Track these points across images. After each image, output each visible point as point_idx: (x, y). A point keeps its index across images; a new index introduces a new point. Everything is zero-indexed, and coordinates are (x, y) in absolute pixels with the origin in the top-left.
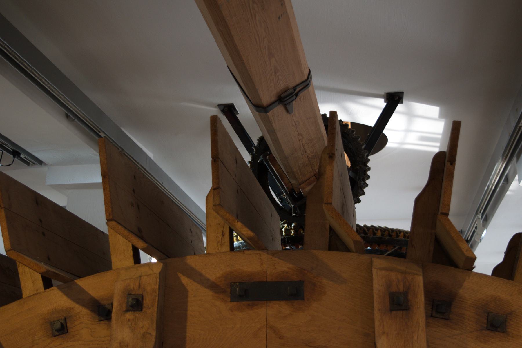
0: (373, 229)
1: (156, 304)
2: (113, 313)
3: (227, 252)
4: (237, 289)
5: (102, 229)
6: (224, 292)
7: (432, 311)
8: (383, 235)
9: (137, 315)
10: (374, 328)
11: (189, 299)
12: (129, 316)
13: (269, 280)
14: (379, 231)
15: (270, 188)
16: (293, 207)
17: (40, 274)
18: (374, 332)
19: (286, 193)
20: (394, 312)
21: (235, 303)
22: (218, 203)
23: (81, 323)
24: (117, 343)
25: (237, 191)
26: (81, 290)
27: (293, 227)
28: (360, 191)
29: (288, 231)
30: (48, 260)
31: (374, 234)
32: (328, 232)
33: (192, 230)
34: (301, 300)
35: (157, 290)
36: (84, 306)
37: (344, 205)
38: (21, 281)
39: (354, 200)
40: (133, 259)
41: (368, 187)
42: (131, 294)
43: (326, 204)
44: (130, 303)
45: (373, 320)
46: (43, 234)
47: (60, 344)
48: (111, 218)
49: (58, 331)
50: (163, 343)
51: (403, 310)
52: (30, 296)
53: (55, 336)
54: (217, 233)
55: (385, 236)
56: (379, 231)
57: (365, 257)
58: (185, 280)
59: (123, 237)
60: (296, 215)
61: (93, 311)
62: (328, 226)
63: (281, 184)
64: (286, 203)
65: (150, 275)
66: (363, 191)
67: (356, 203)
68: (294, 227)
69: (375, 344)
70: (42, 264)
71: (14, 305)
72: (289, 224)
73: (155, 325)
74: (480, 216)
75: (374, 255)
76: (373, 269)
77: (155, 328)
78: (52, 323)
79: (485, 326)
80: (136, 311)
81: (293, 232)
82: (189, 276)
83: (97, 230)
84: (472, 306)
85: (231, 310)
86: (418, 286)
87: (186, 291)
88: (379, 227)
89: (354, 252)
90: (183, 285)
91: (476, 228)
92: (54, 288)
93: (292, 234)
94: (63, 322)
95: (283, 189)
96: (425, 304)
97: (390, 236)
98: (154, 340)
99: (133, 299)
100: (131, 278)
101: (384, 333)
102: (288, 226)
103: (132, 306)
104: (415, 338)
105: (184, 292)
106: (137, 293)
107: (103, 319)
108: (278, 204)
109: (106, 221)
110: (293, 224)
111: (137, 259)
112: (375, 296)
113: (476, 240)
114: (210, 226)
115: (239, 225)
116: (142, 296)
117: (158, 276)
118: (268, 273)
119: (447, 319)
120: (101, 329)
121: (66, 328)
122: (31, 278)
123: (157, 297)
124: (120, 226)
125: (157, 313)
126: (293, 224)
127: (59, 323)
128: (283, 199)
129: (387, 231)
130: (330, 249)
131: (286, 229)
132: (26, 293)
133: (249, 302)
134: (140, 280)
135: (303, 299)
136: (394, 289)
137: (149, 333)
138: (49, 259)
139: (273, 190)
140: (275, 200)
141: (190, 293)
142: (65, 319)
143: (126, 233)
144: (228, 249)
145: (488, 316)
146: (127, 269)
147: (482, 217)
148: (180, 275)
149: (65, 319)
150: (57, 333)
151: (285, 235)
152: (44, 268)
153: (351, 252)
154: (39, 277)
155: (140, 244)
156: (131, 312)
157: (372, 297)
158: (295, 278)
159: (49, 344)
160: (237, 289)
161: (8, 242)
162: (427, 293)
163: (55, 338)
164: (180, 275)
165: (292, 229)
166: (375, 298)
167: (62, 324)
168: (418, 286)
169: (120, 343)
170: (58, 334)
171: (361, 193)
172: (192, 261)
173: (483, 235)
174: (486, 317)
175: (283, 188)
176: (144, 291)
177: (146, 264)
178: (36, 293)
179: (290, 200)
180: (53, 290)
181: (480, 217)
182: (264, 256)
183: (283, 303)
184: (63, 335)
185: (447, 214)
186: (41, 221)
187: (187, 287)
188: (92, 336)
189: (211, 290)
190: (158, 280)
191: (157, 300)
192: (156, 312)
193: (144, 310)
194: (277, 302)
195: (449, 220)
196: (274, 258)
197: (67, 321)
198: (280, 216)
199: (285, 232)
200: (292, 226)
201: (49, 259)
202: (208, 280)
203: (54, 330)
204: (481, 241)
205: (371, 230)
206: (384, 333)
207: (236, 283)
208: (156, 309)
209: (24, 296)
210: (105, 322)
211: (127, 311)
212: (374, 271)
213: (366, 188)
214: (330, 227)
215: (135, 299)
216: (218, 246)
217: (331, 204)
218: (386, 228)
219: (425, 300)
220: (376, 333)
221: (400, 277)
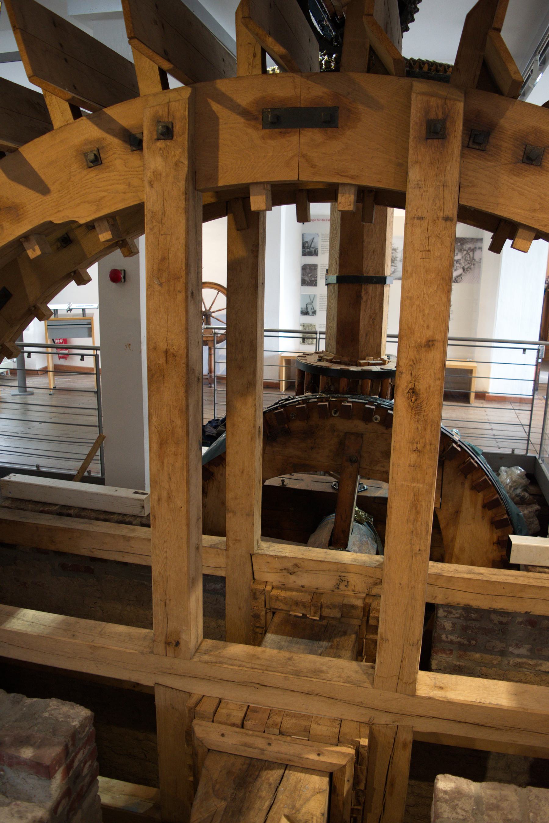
0: (419, 63)
1: (187, 131)
2: (144, 141)
3: (258, 75)
4: (270, 115)
5: (129, 60)
6: (256, 119)
7: (469, 142)
8: (429, 69)
9: (168, 143)
10: (407, 158)
11: (220, 127)
12: (160, 144)
13: (302, 106)
14: (426, 65)
15: (311, 14)
16: (335, 35)
17: (67, 101)
18: (407, 162)
19: (328, 18)
20: (429, 141)
21: (267, 131)
22: (247, 15)
23: (114, 153)
24: (150, 172)
25: (270, 5)
26: (111, 120)
27: (334, 58)
28: (409, 16)
29: (328, 63)
30: (74, 88)
31: (421, 68)
32: (368, 53)
33: (225, 59)
34: (335, 127)
35: (187, 116)
36: (115, 136)
37: (387, 23)
38: (50, 112)
39: (402, 28)
40: (161, 85)
41: (419, 12)
42: (160, 122)
43: (366, 15)
44: (160, 131)
45: (407, 149)
46: (66, 60)
47: (96, 176)
48: (132, 35)
49: (92, 162)
50: (195, 172)
51: (439, 138)
52: (60, 127)
53: (90, 167)
54: (248, 54)
55: (432, 71)
56: (426, 65)
57: (405, 81)
58: (215, 106)
59: (147, 57)
60: (337, 45)
61: (125, 141)
62: (368, 46)
63: (322, 7)
64: (327, 31)
65: (179, 100)
66: (413, 17)
67: (404, 31)
68: (335, 58)
69: (407, 174)
70: (66, 92)
71: (46, 137)
72: (330, 56)
73: (186, 154)
74: (538, 57)
75: (416, 79)
76: (412, 94)
77: (186, 157)
78: (86, 155)
79: (521, 158)
80: (167, 139)
81: (333, 65)
82: (219, 102)
83: (124, 59)
84: (511, 138)
85: (263, 138)
86: (458, 113)
87: (217, 118)
88: (427, 61)
89: (393, 75)
90: (213, 111)
91: (532, 72)
92: (84, 118)
93: (332, 67)
94: (96, 153)
95: (324, 13)
96: (463, 133)
97: (437, 70)
98: (186, 169)
99: (163, 127)
100: (159, 105)
101: (417, 162)
102: (328, 58)
103: (162, 134)
104: (448, 168)
105: (214, 119)
106: (167, 120)
107: (135, 149)
108: (319, 32)
109: (128, 39)
110: (334, 56)
111: (165, 85)
112: (412, 123)
113: (530, 85)
114: (241, 45)
115: (270, 40)
116: (172, 124)
117: (187, 101)
118: (302, 97)
119: (483, 151)
120: (134, 159)
121: (99, 159)
122: (60, 109)
123: (187, 125)
124: (142, 45)
125: (188, 141)
126: (334, 56)
127: (93, 154)
128: (325, 27)
129: (434, 65)
130: (369, 71)
131: (326, 61)
132: (57, 124)
133: (282, 130)
134: (169, 106)
135: (337, 127)
136: (432, 116)
137: (181, 162)
138: (75, 88)
139: (314, 16)
140: (316, 28)
141: (221, 120)
142: (98, 150)
143: (150, 52)
144: (260, 72)
145: (525, 149)
146: (155, 95)
147: (540, 59)
148: (210, 101)
149: (98, 150)
150: (92, 165)
151: (325, 68)
152: (70, 95)
153: (390, 75)
154: (66, 106)
155: (166, 65)
156: (161, 140)
157: (409, 124)
158: (330, 104)
159: (86, 175)
160: (270, 115)
161: (29, 67)
162: (466, 121)
163: (91, 169)
164: (210, 101)
165: (333, 62)
166: (411, 126)
167: (95, 155)
168: (458, 113)
169: (153, 172)
170: (93, 165)
171: (411, 19)
172: (222, 85)
173: (538, 80)
174: (524, 150)
175: (325, 11)
176: (174, 118)
177: (174, 89)
178: (66, 124)
179: (332, 27)
180: (82, 120)
181: (538, 58)
182: (298, 79)
183: (316, 130)
184: (97, 166)
185: (499, 30)
186: (61, 46)
187: (218, 115)
188: (126, 167)
189: (242, 117)
190: (187, 106)
191: (187, 128)
192: (187, 140)
193: (175, 138)
194: (310, 129)
195: (500, 37)
196: (309, 82)
197: (100, 152)
198: (320, 45)
199: (325, 65)
200: (333, 57)
201: (75, 88)
202: (239, 106)
203: (89, 162)
204: (534, 86)
205: (418, 63)
206: (417, 162)
207: (269, 109)
208: (186, 136)
209: (55, 128)
210: (137, 152)
211: (158, 139)
212: (413, 95)
213: (417, 14)
214: (370, 46)
215: (164, 126)
216: (249, 69)
217: (372, 15)
218: (434, 62)
219: (463, 129)
220: (409, 162)
221: (440, 103)
